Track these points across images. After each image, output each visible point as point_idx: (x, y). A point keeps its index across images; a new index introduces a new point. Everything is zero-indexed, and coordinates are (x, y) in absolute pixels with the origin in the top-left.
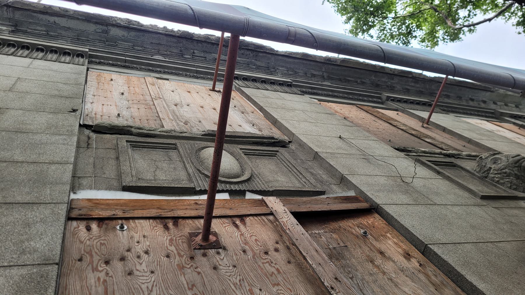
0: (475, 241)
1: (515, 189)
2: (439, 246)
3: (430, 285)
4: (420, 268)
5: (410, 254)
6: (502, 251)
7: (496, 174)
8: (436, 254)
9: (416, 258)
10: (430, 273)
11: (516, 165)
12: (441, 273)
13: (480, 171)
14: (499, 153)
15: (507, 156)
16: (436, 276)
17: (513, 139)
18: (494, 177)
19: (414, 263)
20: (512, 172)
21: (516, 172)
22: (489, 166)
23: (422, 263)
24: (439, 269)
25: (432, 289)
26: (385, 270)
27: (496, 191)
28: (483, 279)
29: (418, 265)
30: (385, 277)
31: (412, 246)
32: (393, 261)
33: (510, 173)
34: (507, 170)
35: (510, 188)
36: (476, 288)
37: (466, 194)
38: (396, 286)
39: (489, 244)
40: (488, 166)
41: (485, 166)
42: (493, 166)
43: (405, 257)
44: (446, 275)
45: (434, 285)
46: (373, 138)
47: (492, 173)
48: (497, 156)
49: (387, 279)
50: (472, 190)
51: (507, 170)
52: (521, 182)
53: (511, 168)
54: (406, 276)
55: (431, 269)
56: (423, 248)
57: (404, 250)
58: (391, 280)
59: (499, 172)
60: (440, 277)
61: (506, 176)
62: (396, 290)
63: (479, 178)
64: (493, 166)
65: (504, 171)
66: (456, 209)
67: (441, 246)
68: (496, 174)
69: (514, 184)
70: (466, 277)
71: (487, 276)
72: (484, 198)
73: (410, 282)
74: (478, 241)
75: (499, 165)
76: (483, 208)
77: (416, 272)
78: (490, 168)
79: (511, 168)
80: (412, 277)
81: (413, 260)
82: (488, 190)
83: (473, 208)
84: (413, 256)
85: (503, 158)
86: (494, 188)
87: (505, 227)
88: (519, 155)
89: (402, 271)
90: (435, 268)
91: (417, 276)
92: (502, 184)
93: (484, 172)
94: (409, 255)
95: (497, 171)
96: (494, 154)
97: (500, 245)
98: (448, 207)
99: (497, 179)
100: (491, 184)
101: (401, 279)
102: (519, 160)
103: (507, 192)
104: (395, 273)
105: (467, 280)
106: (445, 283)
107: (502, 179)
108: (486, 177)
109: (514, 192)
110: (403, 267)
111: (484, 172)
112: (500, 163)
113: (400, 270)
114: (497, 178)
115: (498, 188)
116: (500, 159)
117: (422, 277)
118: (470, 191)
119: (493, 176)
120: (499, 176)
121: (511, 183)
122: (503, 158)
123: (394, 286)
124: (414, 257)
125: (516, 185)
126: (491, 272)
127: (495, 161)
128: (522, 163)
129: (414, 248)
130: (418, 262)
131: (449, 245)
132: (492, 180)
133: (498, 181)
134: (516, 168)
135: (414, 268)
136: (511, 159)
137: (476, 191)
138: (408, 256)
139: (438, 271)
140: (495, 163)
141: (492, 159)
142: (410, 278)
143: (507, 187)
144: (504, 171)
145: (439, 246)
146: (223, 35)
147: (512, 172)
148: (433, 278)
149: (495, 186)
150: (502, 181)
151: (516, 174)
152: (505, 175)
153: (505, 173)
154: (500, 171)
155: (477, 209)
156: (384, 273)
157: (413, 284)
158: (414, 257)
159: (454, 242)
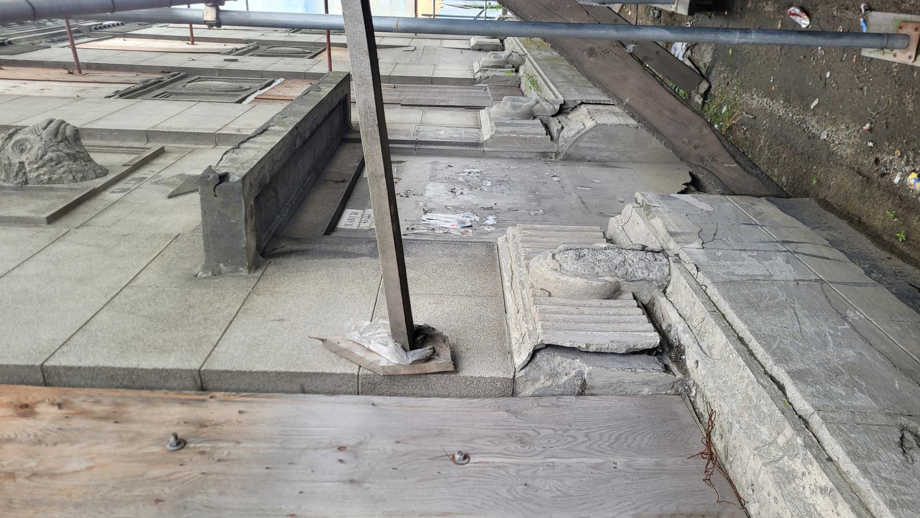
0: (105, 301)
1: (84, 179)
2: (63, 353)
3: (103, 423)
4: (64, 411)
5: (26, 402)
6: (150, 289)
7: (38, 168)
8: (71, 368)
9: (43, 401)
10: (86, 406)
11: (59, 139)
12: (101, 391)
13: (7, 176)
14: (18, 130)
15: (34, 131)
16: (97, 402)
17: (8, 93)
18: (38, 176)
19: (47, 412)
20: (61, 154)
21: (67, 151)
22: (17, 161)
23: (58, 400)
24: (93, 387)
25: (111, 426)
26: (10, 469)
27: (59, 197)
28: (163, 351)
29: (55, 409)
30: (20, 480)
31: (19, 387)
32: (9, 440)
33: (58, 156)
34: (50, 154)
35: (75, 180)
36: (167, 370)
37: (23, 232)
38: (52, 476)
39: (126, 291)
40: (16, 161)
41: (10, 164)
42: (23, 158)
43: (24, 415)
44: (110, 387)
45: (106, 418)
46: (808, 249)
47: (30, 171)
48: (17, 138)
49: (26, 482)
50: (23, 218)
51: (50, 154)
52: (84, 163)
53: (54, 148)
54: (55, 444)
55: (80, 398)
56: (39, 376)
57: (9, 405)
58: (35, 474)
59: (40, 163)
60: (106, 400)
61: (57, 164)
62: (59, 483)
63: (14, 188)
64: (23, 158)
65: (46, 157)
66: (31, 268)
67: (65, 349)
68: (38, 168)
69: (77, 171)
70: (141, 367)
71: (165, 341)
72: (53, 219)
73: (68, 449)
74: (109, 298)
75: (34, 151)
76: (68, 238)
77: (63, 424)
78: (22, 163)
79: (54, 148)
80: (65, 437)
81: (42, 409)
82: (47, 203)
83: (54, 249)
84: (34, 401)
85: (31, 137)
86: (52, 193)
87: (123, 249)
88: (51, 121)
89: (40, 442)
90: (86, 391)
91: (71, 430)
92: (60, 180)
93: (17, 175)
94: (27, 406)
95: (36, 163)
96: (11, 136)
97: (139, 281)
98: (16, 272)
99: (46, 177)
100: (42, 189)
101: (50, 457)
102: (58, 129)
103: (76, 189)
104: (30, 456)
105: (147, 370)
106: (119, 401)
107: (54, 172)
108: (26, 182)
109: (85, 183)
110: (35, 436)
111: (17, 175)
112: (32, 147)
113: (35, 444)
114: (44, 174)
115: (58, 189)
116: (27, 140)
117: (80, 422)
118: (22, 222)
119: (35, 174)
120: (45, 169)
121: (70, 172)
122: (31, 137)
123: (49, 481)
124: (38, 402)
125: (81, 171)
126: (164, 331)
127: (21, 147)
128: (64, 133)
129: (24, 387)
130: (52, 404)
131: (76, 337)
132: (39, 183)
133: (50, 179)
134: (62, 144)
135: (54, 420)
136: (44, 133)
137: (32, 215)
138: (25, 410)
139: (95, 392)
140: (22, 151)
141: (13, 147)
142: (63, 442)
143: (70, 181)
144: (46, 157)
145: (63, 353)
146: (676, 8)
147: (61, 154)
148: (97, 409)
149: (51, 189)
150: (55, 177)
151: (68, 154)
152: (53, 163)
153: (51, 160)
154: (41, 161)
155: (60, 248)
156: (12, 475)
157: (76, 446)
158: (38, 402)
159: (78, 326)
